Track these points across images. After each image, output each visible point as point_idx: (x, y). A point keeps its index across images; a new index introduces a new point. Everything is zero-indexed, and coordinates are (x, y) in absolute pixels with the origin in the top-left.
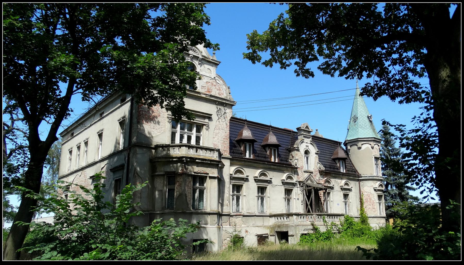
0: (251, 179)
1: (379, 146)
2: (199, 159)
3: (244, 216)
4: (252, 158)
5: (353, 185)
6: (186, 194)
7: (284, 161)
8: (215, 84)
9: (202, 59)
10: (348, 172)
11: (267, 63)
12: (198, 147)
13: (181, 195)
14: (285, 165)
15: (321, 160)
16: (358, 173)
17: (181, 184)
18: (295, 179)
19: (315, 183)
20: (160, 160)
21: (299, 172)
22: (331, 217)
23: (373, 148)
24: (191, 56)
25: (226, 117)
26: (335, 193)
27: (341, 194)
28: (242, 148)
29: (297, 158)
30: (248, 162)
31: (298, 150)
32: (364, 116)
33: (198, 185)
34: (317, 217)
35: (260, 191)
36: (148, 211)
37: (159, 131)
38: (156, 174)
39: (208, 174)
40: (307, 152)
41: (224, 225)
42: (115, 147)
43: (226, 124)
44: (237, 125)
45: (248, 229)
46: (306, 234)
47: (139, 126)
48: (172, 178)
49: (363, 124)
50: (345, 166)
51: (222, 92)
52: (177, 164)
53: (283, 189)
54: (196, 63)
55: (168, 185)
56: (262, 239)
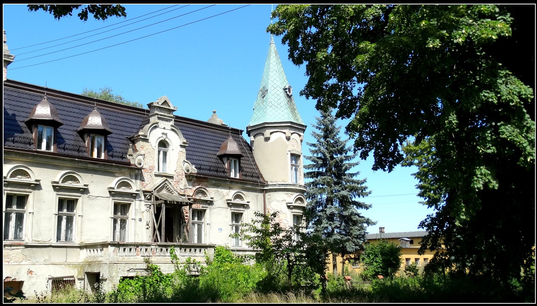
1: (300, 136)
3: (27, 246)
4: (238, 177)
5: (252, 198)
7: (249, 176)
10: (244, 178)
14: (117, 163)
15: (189, 158)
16: (263, 179)
18: (135, 186)
19: (176, 194)
21: (146, 175)
22: (188, 250)
23: (288, 139)
26: (214, 211)
27: (228, 212)
28: (226, 165)
29: (143, 152)
30: (41, 157)
31: (146, 140)
32: (278, 88)
34: (159, 249)
35: (234, 219)
40: (163, 144)
45: (32, 268)
46: (132, 278)
49: (276, 100)
50: (240, 168)
53: (110, 203)
56: (58, 283)
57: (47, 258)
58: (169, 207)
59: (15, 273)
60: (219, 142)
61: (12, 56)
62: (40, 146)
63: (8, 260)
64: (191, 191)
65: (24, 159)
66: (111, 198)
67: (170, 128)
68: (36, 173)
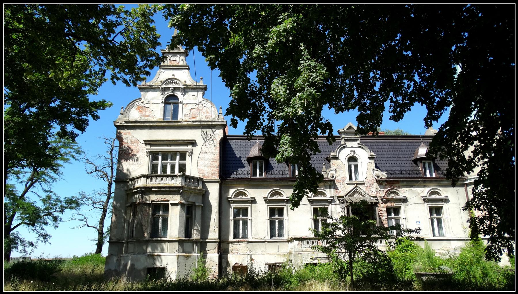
0: (260, 201)
2: (155, 187)
3: (249, 242)
4: (434, 176)
21: (338, 185)
26: (408, 207)
29: (334, 168)
31: (337, 159)
39: (169, 201)
40: (352, 159)
41: (210, 253)
53: (426, 207)
54: (178, 94)
57: (264, 250)
58: (355, 207)
59: (241, 260)
60: (413, 150)
62: (426, 175)
64: (382, 193)
66: (310, 205)
67: (357, 145)
68: (251, 193)
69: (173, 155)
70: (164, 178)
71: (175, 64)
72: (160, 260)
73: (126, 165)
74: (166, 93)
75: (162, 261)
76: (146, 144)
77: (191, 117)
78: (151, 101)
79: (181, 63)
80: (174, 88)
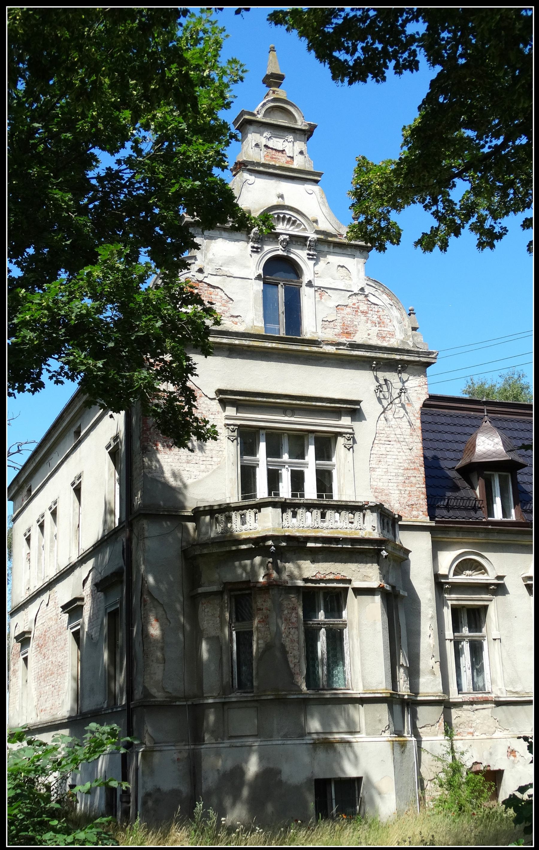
2: (316, 539)
3: (499, 704)
4: (513, 517)
6: (283, 646)
8: (363, 307)
9: (319, 240)
11: (427, 242)
12: (325, 505)
13: (268, 648)
17: (267, 617)
20: (205, 551)
24: (282, 238)
25: (410, 403)
28: (478, 491)
30: (500, 532)
33: (321, 616)
36: (186, 698)
37: (203, 467)
38: (200, 590)
39: (349, 581)
41: (427, 734)
42: (105, 522)
43: (411, 424)
44: (463, 421)
47: (146, 460)
48: (242, 598)
51: (391, 329)
52: (252, 558)
54: (300, 255)
55: (237, 620)
59: (486, 754)
61: (433, 353)
62: (491, 513)
63: (471, 730)
65: (470, 539)
69: (298, 442)
70: (329, 514)
71: (282, 161)
72: (352, 756)
73: (170, 460)
74: (267, 248)
75: (356, 757)
76: (224, 403)
77: (338, 330)
78: (225, 269)
79: (299, 163)
80: (291, 236)
